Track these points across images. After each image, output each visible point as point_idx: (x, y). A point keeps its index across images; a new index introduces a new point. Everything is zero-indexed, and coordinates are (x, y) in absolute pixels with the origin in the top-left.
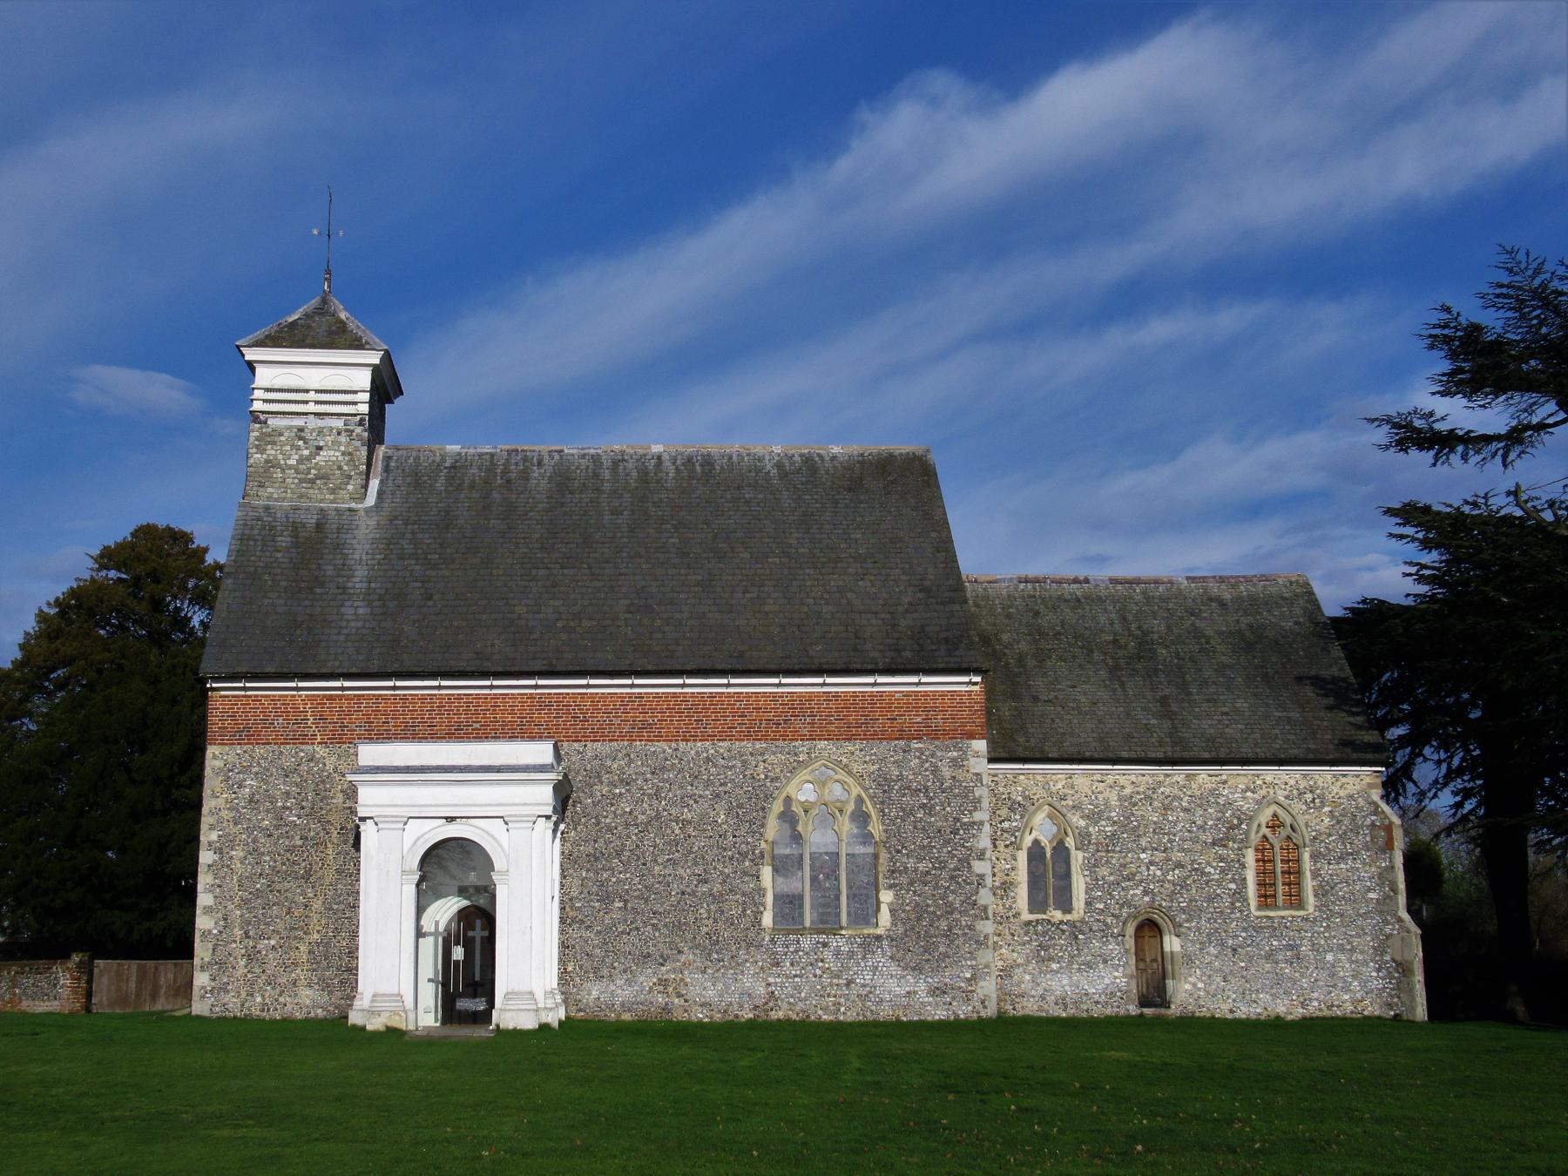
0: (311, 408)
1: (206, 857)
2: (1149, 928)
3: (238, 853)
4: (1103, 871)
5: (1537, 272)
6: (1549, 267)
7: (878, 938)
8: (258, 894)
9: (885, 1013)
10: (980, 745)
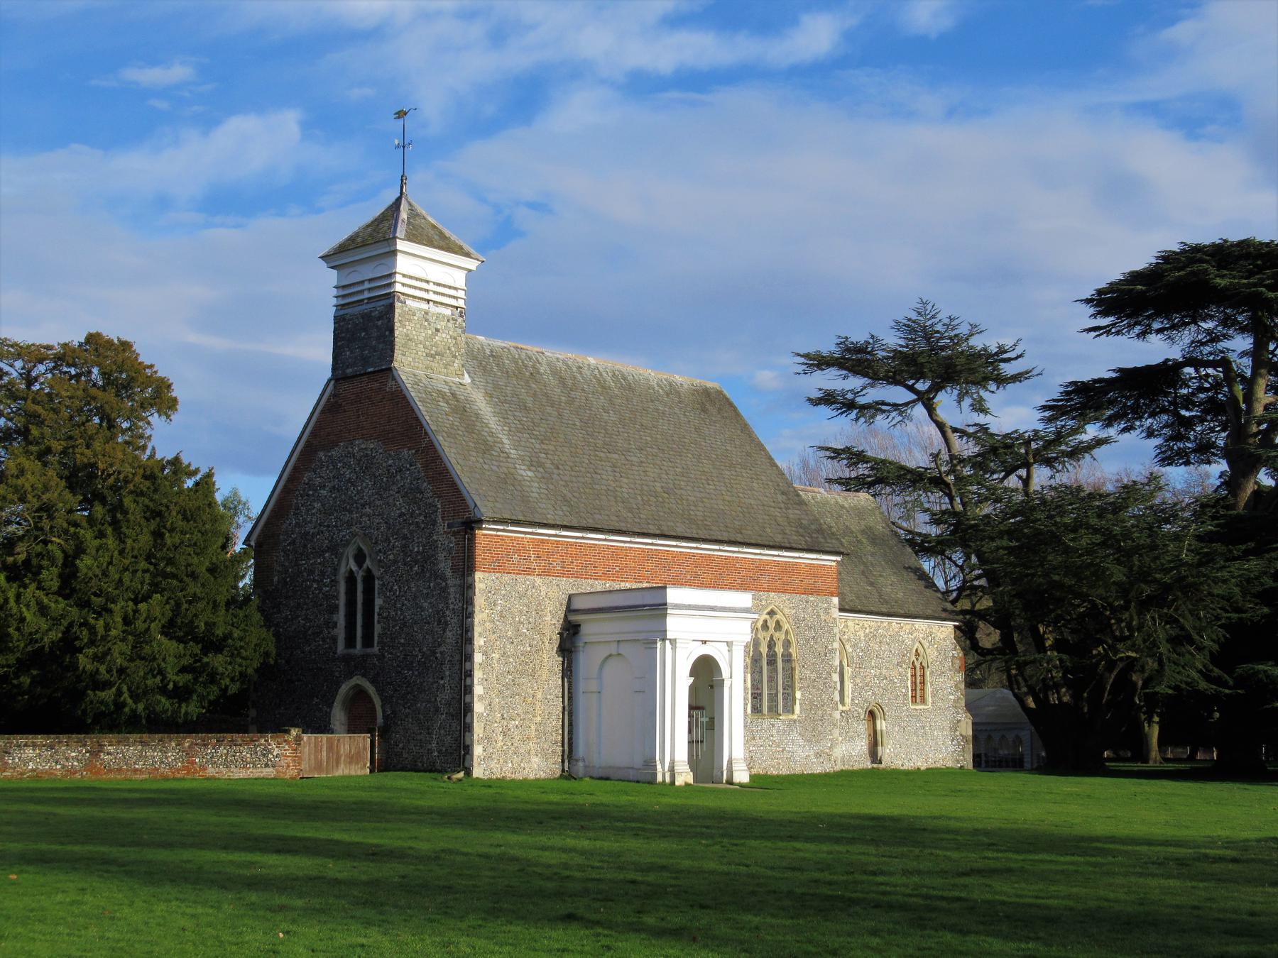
0: (431, 296)
1: (478, 658)
2: (872, 714)
3: (496, 656)
4: (858, 680)
5: (933, 317)
6: (939, 316)
7: (795, 721)
8: (507, 686)
9: (798, 771)
10: (835, 600)
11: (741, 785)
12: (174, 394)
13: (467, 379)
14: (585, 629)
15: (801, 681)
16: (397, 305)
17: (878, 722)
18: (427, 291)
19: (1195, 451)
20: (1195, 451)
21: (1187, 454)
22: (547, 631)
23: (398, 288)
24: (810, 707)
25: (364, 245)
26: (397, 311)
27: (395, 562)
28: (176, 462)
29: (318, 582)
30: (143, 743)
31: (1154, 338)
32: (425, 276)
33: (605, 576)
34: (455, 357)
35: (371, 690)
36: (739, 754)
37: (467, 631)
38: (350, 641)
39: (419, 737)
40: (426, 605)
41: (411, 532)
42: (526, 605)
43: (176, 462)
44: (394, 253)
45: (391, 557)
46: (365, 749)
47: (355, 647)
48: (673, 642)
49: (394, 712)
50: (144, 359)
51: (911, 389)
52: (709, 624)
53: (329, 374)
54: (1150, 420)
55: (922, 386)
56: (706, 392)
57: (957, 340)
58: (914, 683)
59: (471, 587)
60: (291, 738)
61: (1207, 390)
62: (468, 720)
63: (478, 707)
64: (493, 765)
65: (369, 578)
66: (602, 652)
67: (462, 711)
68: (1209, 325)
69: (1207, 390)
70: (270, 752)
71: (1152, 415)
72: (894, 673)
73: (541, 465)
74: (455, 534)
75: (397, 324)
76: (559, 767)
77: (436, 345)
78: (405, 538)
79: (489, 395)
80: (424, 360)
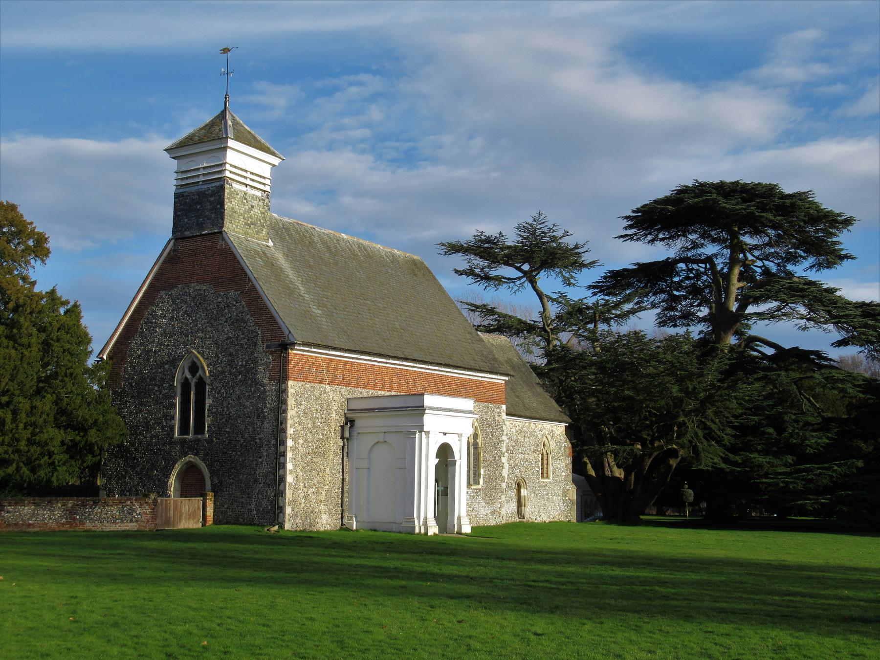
0: (248, 182)
1: (290, 443)
2: (519, 486)
3: (301, 441)
4: (512, 462)
5: (542, 223)
6: (546, 224)
8: (308, 464)
10: (504, 407)
11: (466, 534)
12: (48, 246)
13: (271, 244)
14: (358, 423)
15: (489, 461)
16: (227, 186)
17: (522, 490)
18: (246, 178)
19: (680, 318)
20: (680, 318)
21: (675, 320)
22: (333, 424)
23: (227, 174)
24: (490, 480)
25: (201, 141)
26: (227, 191)
27: (223, 372)
28: (52, 293)
29: (159, 386)
30: (36, 504)
31: (659, 244)
32: (246, 166)
33: (369, 386)
34: (263, 226)
35: (202, 466)
36: (467, 513)
37: (282, 423)
38: (184, 429)
39: (241, 500)
40: (248, 404)
41: (237, 351)
42: (320, 405)
43: (52, 293)
44: (225, 148)
45: (220, 369)
46: (199, 508)
47: (203, 433)
48: (428, 433)
49: (220, 482)
50: (27, 218)
51: (519, 269)
52: (449, 421)
53: (170, 235)
54: (653, 297)
55: (526, 267)
56: (414, 262)
57: (554, 239)
58: (542, 464)
59: (285, 391)
60: (150, 501)
61: (691, 278)
62: (281, 488)
63: (290, 479)
64: (298, 520)
65: (201, 384)
66: (372, 439)
67: (277, 481)
68: (693, 237)
69: (691, 278)
70: (134, 511)
71: (655, 294)
72: (532, 457)
73: (325, 306)
74: (272, 353)
75: (226, 200)
76: (339, 522)
77: (251, 217)
78: (231, 355)
79: (286, 256)
80: (243, 228)
